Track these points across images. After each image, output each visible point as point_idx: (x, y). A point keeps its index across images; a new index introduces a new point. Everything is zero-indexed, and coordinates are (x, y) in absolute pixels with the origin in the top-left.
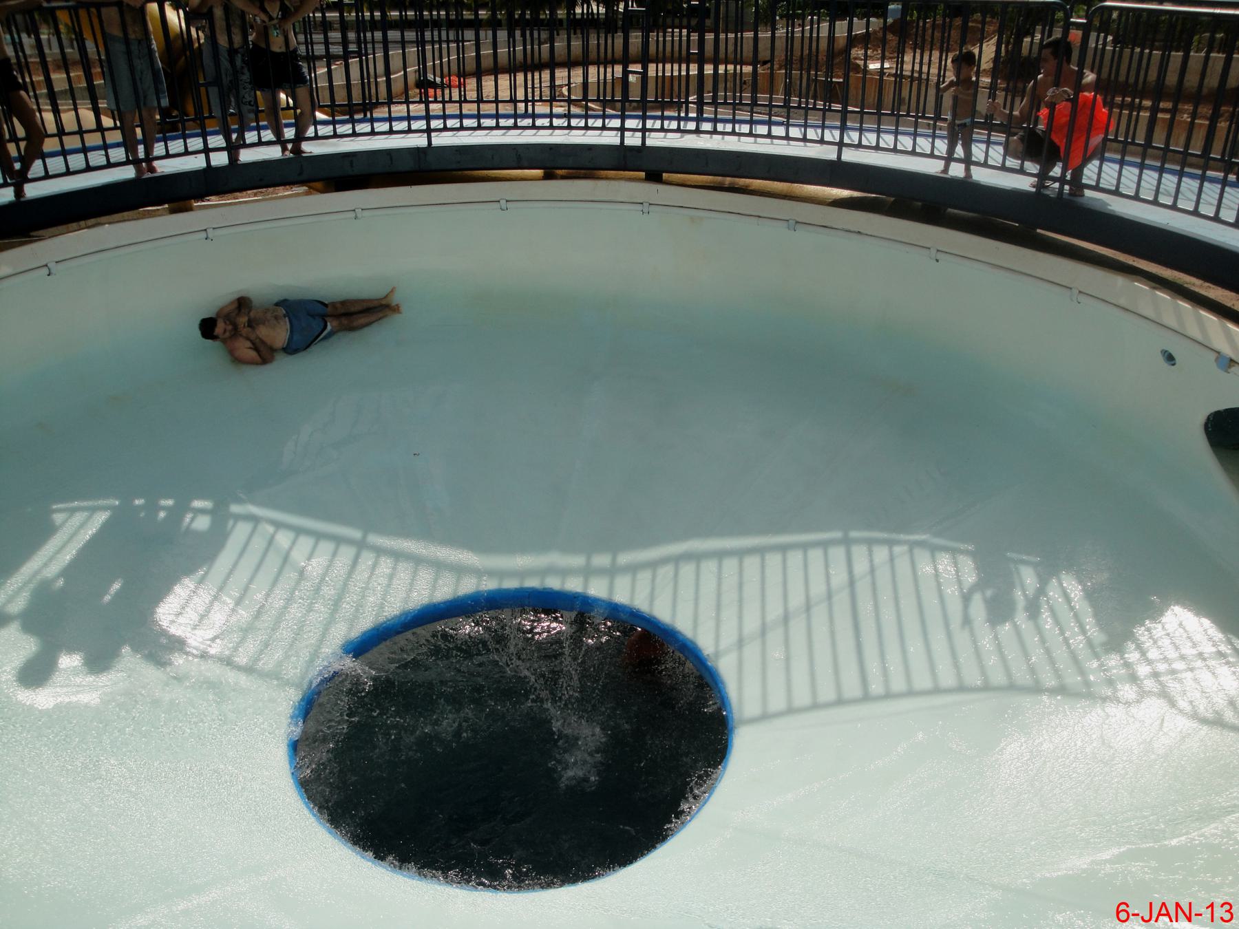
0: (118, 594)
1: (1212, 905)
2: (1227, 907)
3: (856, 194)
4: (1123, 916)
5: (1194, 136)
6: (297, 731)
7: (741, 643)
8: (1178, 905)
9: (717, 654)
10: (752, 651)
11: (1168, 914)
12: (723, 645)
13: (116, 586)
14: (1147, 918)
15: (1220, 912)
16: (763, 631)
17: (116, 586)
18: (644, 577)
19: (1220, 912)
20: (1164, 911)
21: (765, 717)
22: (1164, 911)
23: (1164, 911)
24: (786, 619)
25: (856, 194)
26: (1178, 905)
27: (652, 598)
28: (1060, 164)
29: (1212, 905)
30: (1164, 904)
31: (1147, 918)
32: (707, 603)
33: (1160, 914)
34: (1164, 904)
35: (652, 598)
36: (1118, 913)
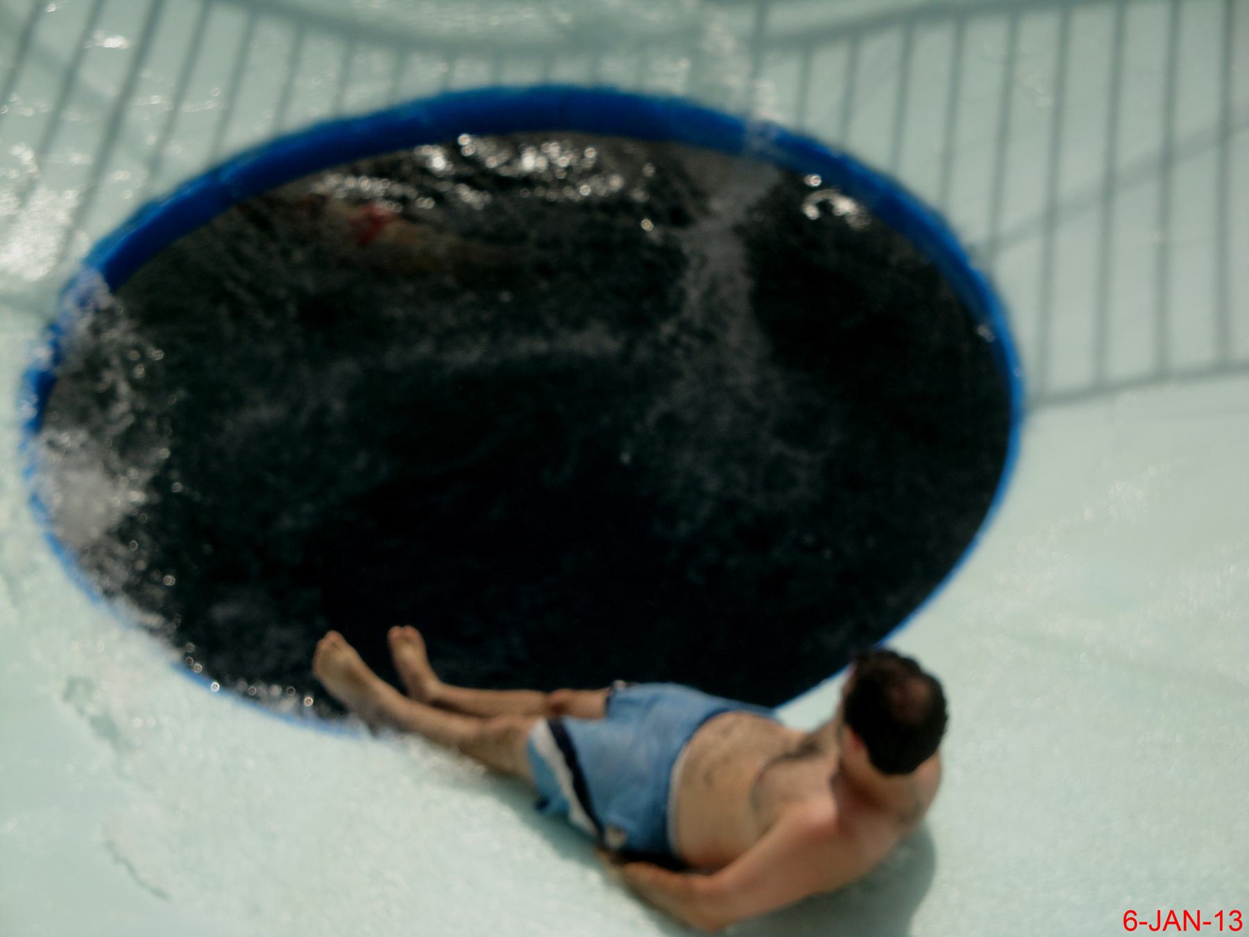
1: (1221, 913)
2: (1236, 915)
4: (1131, 924)
6: (362, 728)
7: (1051, 217)
8: (1186, 913)
9: (995, 244)
10: (1077, 241)
11: (1176, 922)
12: (1012, 218)
14: (1154, 926)
15: (1228, 920)
16: (1110, 187)
18: (829, 64)
19: (1228, 920)
20: (1172, 919)
21: (1100, 389)
22: (1172, 919)
23: (1172, 920)
24: (1166, 161)
26: (1186, 913)
27: (847, 112)
29: (1221, 913)
30: (1172, 912)
31: (1154, 926)
32: (977, 124)
33: (1168, 923)
34: (1172, 912)
35: (847, 112)
36: (1125, 921)
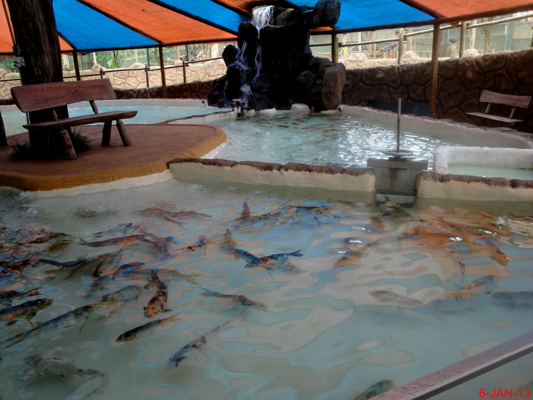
0: (456, 241)
1: (521, 390)
3: (41, 124)
4: (482, 394)
5: (34, 331)
8: (506, 390)
11: (502, 394)
13: (458, 239)
15: (524, 393)
17: (458, 239)
19: (524, 393)
20: (500, 393)
22: (500, 393)
25: (41, 124)
26: (506, 390)
28: (461, 239)
29: (521, 390)
30: (500, 389)
33: (498, 394)
34: (500, 389)
36: (480, 393)
